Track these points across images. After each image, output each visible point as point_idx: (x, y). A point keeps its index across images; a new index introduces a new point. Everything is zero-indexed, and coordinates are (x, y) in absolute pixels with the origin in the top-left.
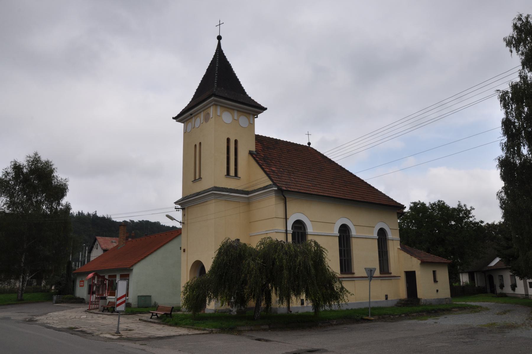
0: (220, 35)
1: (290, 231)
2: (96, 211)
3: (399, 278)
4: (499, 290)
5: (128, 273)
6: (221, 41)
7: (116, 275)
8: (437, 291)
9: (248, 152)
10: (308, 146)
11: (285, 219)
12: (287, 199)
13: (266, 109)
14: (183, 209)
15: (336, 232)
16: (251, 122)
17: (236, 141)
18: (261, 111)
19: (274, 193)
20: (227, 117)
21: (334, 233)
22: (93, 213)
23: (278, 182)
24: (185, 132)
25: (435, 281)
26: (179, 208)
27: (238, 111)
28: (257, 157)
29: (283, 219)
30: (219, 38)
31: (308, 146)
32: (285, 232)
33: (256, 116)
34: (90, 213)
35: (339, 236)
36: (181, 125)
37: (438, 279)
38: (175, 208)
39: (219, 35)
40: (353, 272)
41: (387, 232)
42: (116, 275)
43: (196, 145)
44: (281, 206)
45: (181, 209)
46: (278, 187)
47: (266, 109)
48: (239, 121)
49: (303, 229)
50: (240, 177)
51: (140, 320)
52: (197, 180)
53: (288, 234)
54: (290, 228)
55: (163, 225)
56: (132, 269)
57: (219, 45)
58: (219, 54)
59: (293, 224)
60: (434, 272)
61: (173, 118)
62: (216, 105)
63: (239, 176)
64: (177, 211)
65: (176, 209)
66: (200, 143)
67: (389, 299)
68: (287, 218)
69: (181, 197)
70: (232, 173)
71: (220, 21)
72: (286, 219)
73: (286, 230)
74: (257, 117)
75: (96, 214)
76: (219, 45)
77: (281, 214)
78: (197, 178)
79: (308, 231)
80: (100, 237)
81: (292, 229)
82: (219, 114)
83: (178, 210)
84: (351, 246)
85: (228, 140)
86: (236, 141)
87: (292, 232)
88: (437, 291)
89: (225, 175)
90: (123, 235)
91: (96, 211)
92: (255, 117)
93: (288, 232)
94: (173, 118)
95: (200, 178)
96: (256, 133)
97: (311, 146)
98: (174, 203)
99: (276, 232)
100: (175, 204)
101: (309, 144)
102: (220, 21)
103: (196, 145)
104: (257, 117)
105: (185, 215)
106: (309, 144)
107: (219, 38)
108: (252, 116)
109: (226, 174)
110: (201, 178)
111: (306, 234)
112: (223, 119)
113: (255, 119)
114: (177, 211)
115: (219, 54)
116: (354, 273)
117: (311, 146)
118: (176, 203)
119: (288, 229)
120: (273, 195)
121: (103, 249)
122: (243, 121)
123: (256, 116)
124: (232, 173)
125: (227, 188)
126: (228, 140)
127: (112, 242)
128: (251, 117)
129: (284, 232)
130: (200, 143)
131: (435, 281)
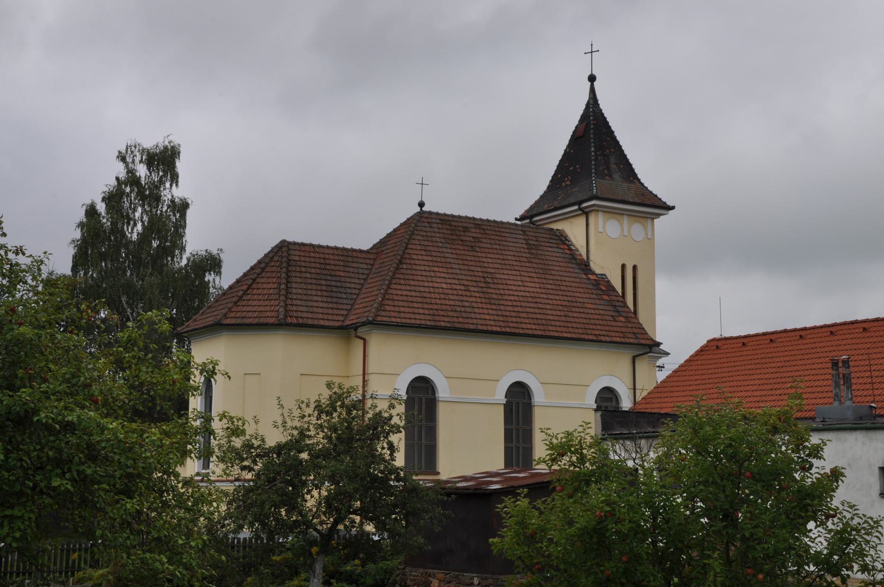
0: (593, 73)
6: (595, 83)
15: (500, 396)
17: (635, 268)
21: (586, 403)
23: (609, 323)
27: (628, 215)
29: (369, 372)
30: (592, 79)
35: (504, 404)
39: (590, 73)
40: (437, 471)
41: (620, 397)
47: (673, 208)
49: (430, 392)
57: (592, 91)
71: (592, 45)
76: (592, 91)
79: (536, 400)
84: (437, 419)
85: (623, 266)
86: (635, 268)
102: (592, 45)
107: (592, 79)
112: (607, 231)
116: (438, 473)
122: (637, 230)
126: (623, 266)
128: (649, 221)
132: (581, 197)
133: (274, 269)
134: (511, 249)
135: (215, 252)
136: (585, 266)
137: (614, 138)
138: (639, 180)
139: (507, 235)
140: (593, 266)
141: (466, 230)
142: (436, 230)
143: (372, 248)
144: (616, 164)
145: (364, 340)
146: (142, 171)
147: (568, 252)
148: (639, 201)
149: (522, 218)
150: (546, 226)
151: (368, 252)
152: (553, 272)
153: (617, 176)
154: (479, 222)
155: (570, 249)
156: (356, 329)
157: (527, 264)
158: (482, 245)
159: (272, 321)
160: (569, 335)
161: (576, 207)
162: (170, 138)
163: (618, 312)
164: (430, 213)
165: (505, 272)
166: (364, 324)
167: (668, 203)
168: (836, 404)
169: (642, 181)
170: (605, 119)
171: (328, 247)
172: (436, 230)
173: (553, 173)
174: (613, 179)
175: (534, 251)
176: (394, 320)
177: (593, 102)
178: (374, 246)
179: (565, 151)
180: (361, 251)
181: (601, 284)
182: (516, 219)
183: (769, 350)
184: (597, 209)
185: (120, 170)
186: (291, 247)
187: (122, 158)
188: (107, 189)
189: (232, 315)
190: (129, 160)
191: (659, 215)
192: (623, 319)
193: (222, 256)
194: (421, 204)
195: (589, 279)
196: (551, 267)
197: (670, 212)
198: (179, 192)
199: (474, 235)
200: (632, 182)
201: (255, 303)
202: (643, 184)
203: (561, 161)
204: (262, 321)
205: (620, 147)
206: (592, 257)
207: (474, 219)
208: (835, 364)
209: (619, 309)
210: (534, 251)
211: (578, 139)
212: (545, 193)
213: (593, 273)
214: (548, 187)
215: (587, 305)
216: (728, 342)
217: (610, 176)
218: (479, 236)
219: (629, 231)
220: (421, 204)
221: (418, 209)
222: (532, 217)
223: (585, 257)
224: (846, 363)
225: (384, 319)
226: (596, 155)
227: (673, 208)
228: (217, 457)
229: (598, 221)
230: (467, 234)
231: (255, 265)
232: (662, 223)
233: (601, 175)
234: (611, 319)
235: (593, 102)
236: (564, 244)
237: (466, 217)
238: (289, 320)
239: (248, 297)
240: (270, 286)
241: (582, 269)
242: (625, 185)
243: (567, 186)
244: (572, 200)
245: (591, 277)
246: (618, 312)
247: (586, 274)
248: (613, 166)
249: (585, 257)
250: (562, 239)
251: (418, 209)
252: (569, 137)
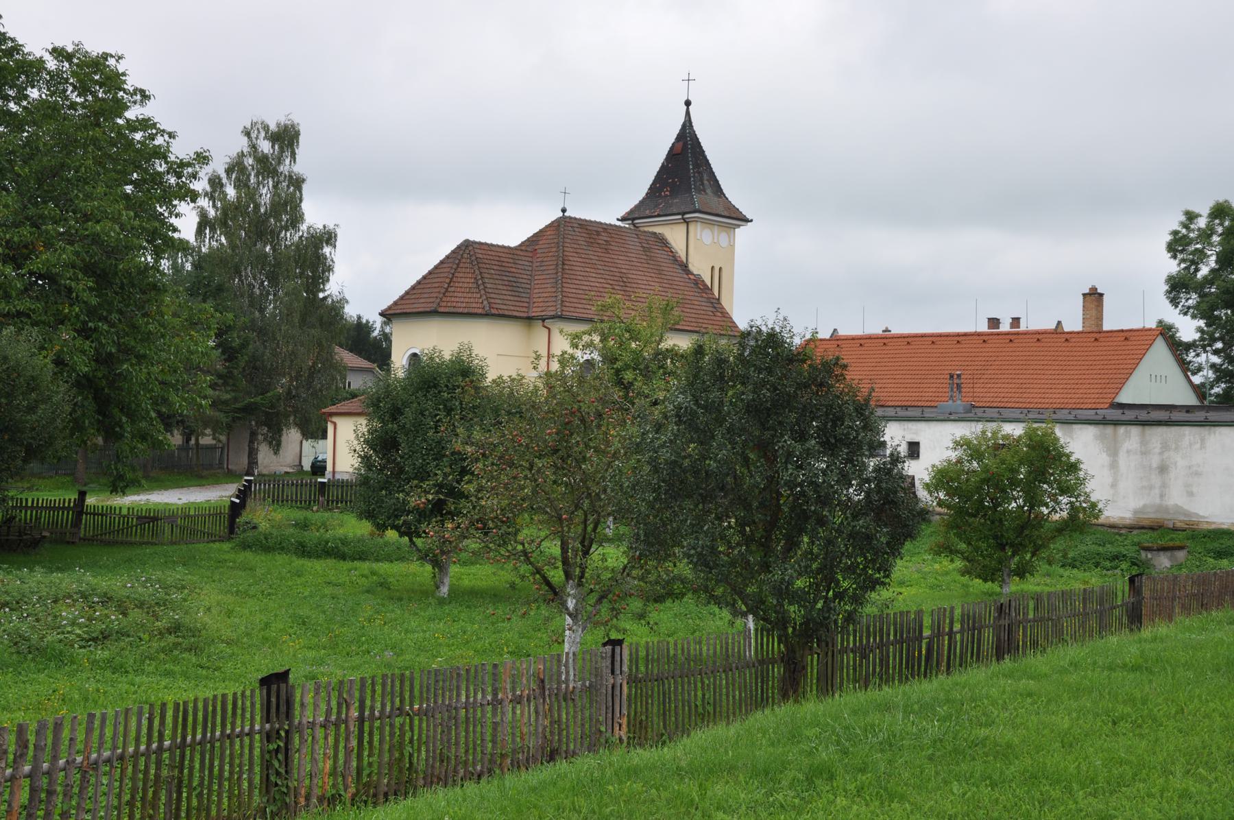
17: (720, 269)
30: (688, 103)
47: (751, 221)
57: (688, 113)
76: (688, 113)
85: (713, 267)
86: (720, 269)
107: (688, 103)
122: (723, 238)
126: (713, 267)
132: (683, 209)
133: (466, 265)
134: (632, 251)
135: (331, 227)
136: (685, 267)
137: (705, 157)
138: (724, 195)
139: (627, 238)
140: (691, 267)
141: (598, 233)
142: (578, 234)
143: (521, 245)
144: (708, 180)
145: (549, 329)
146: (265, 146)
147: (671, 254)
148: (728, 215)
149: (623, 219)
150: (646, 229)
151: (516, 248)
152: (665, 273)
153: (709, 191)
154: (605, 227)
155: (672, 252)
156: (543, 320)
157: (646, 265)
158: (611, 247)
159: (480, 311)
160: (689, 328)
161: (680, 217)
162: (290, 117)
163: (715, 308)
164: (570, 218)
165: (634, 272)
166: (553, 317)
167: (747, 217)
168: (951, 402)
169: (727, 196)
170: (698, 139)
171: (498, 246)
172: (578, 234)
173: (651, 182)
174: (706, 194)
175: (648, 253)
176: (574, 314)
177: (687, 126)
178: (522, 243)
179: (663, 164)
180: (509, 248)
181: (698, 282)
182: (618, 220)
183: (860, 352)
184: (696, 220)
185: (242, 144)
186: (475, 246)
187: (248, 134)
188: (229, 160)
189: (444, 304)
190: (254, 135)
191: (739, 226)
192: (719, 314)
193: (339, 231)
194: (564, 211)
195: (690, 279)
196: (663, 268)
197: (749, 223)
198: (298, 169)
199: (605, 239)
200: (720, 197)
201: (460, 295)
202: (727, 199)
203: (658, 173)
204: (471, 311)
205: (710, 165)
206: (690, 260)
207: (601, 223)
208: (952, 376)
209: (716, 305)
210: (648, 253)
211: (673, 155)
212: (644, 199)
213: (693, 274)
214: (647, 194)
215: (694, 302)
216: (822, 342)
217: (705, 191)
218: (609, 239)
219: (718, 239)
220: (564, 211)
221: (561, 214)
222: (633, 219)
223: (685, 261)
224: (959, 376)
225: (568, 314)
226: (694, 173)
227: (751, 221)
228: (984, 432)
229: (696, 229)
230: (600, 237)
231: (444, 259)
232: (742, 233)
233: (699, 191)
234: (711, 314)
235: (687, 126)
236: (667, 246)
237: (595, 222)
238: (493, 311)
239: (452, 289)
240: (468, 280)
241: (684, 270)
242: (716, 199)
243: (666, 196)
244: (675, 211)
245: (692, 277)
246: (715, 308)
247: (687, 274)
248: (706, 182)
249: (685, 261)
250: (663, 242)
251: (561, 214)
252: (666, 153)
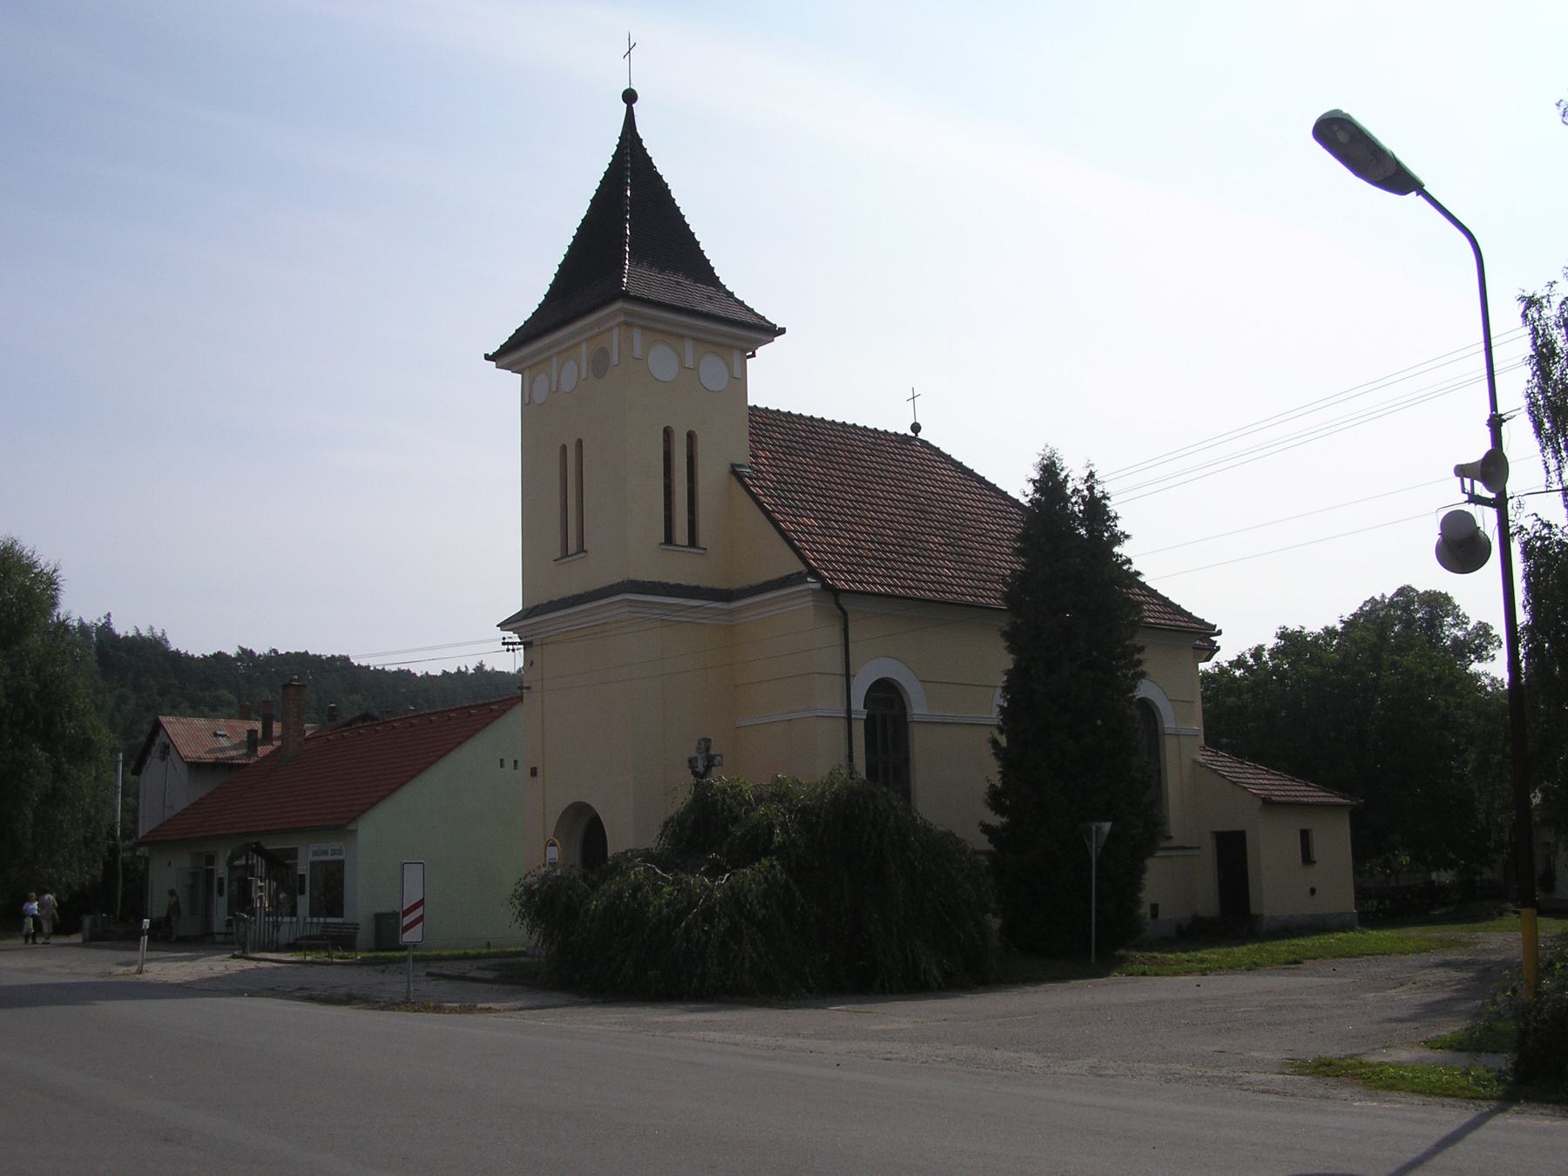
1: (858, 712)
2: (109, 614)
3: (1197, 852)
4: (1539, 896)
5: (295, 846)
7: (296, 849)
8: (1313, 891)
9: (726, 469)
10: (913, 435)
11: (844, 679)
12: (849, 616)
13: (782, 331)
14: (527, 645)
16: (737, 374)
17: (691, 436)
18: (764, 337)
19: (811, 598)
20: (663, 361)
22: (99, 620)
24: (527, 402)
25: (1307, 859)
26: (515, 641)
28: (755, 486)
30: (630, 97)
31: (913, 435)
32: (846, 716)
33: (751, 353)
34: (87, 621)
36: (513, 381)
37: (1317, 852)
38: (504, 644)
39: (628, 87)
42: (296, 849)
43: (564, 448)
44: (833, 634)
45: (520, 644)
46: (821, 579)
47: (782, 331)
48: (698, 373)
50: (705, 549)
51: (428, 974)
52: (572, 555)
53: (853, 723)
54: (858, 704)
55: (363, 664)
56: (356, 830)
58: (630, 145)
59: (867, 693)
60: (1305, 835)
61: (487, 357)
62: (628, 325)
63: (701, 546)
64: (508, 650)
65: (506, 647)
66: (580, 443)
67: (1161, 916)
68: (852, 673)
69: (521, 608)
70: (681, 534)
72: (848, 676)
73: (849, 711)
74: (753, 355)
75: (108, 622)
77: (831, 659)
78: (572, 547)
79: (915, 712)
80: (171, 719)
81: (865, 708)
82: (638, 352)
83: (511, 647)
85: (668, 433)
86: (691, 436)
87: (865, 717)
88: (1313, 891)
89: (661, 544)
90: (296, 719)
91: (109, 614)
92: (748, 354)
93: (853, 716)
94: (487, 357)
95: (581, 549)
96: (751, 403)
97: (921, 435)
98: (498, 626)
99: (818, 716)
100: (501, 630)
101: (916, 428)
103: (564, 448)
104: (753, 355)
105: (534, 664)
106: (916, 428)
107: (630, 97)
108: (739, 352)
109: (663, 541)
110: (586, 551)
111: (909, 720)
113: (748, 360)
114: (508, 650)
115: (630, 145)
117: (921, 435)
118: (503, 625)
119: (853, 707)
120: (808, 602)
121: (187, 762)
122: (712, 370)
123: (751, 353)
124: (681, 534)
125: (667, 584)
126: (668, 433)
127: (216, 735)
128: (736, 355)
129: (843, 715)
130: (580, 443)
131: (1307, 859)
